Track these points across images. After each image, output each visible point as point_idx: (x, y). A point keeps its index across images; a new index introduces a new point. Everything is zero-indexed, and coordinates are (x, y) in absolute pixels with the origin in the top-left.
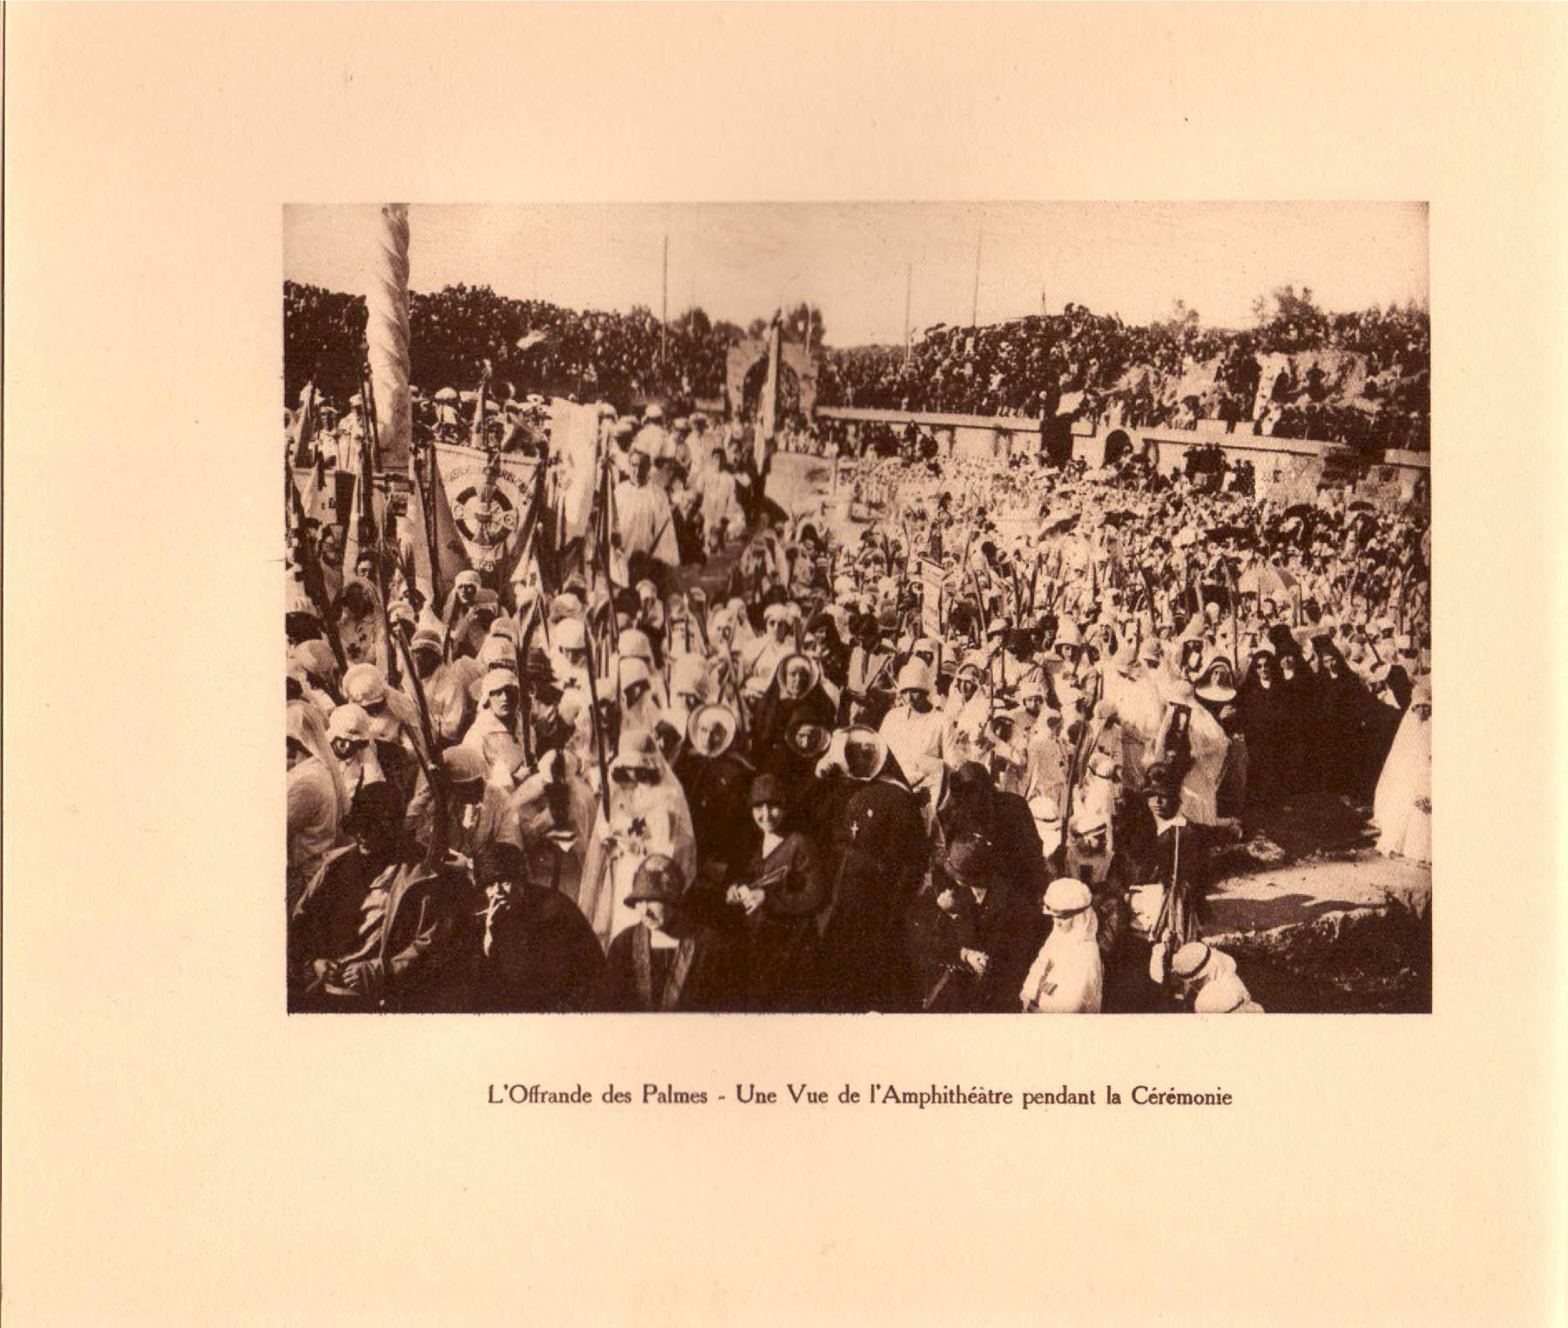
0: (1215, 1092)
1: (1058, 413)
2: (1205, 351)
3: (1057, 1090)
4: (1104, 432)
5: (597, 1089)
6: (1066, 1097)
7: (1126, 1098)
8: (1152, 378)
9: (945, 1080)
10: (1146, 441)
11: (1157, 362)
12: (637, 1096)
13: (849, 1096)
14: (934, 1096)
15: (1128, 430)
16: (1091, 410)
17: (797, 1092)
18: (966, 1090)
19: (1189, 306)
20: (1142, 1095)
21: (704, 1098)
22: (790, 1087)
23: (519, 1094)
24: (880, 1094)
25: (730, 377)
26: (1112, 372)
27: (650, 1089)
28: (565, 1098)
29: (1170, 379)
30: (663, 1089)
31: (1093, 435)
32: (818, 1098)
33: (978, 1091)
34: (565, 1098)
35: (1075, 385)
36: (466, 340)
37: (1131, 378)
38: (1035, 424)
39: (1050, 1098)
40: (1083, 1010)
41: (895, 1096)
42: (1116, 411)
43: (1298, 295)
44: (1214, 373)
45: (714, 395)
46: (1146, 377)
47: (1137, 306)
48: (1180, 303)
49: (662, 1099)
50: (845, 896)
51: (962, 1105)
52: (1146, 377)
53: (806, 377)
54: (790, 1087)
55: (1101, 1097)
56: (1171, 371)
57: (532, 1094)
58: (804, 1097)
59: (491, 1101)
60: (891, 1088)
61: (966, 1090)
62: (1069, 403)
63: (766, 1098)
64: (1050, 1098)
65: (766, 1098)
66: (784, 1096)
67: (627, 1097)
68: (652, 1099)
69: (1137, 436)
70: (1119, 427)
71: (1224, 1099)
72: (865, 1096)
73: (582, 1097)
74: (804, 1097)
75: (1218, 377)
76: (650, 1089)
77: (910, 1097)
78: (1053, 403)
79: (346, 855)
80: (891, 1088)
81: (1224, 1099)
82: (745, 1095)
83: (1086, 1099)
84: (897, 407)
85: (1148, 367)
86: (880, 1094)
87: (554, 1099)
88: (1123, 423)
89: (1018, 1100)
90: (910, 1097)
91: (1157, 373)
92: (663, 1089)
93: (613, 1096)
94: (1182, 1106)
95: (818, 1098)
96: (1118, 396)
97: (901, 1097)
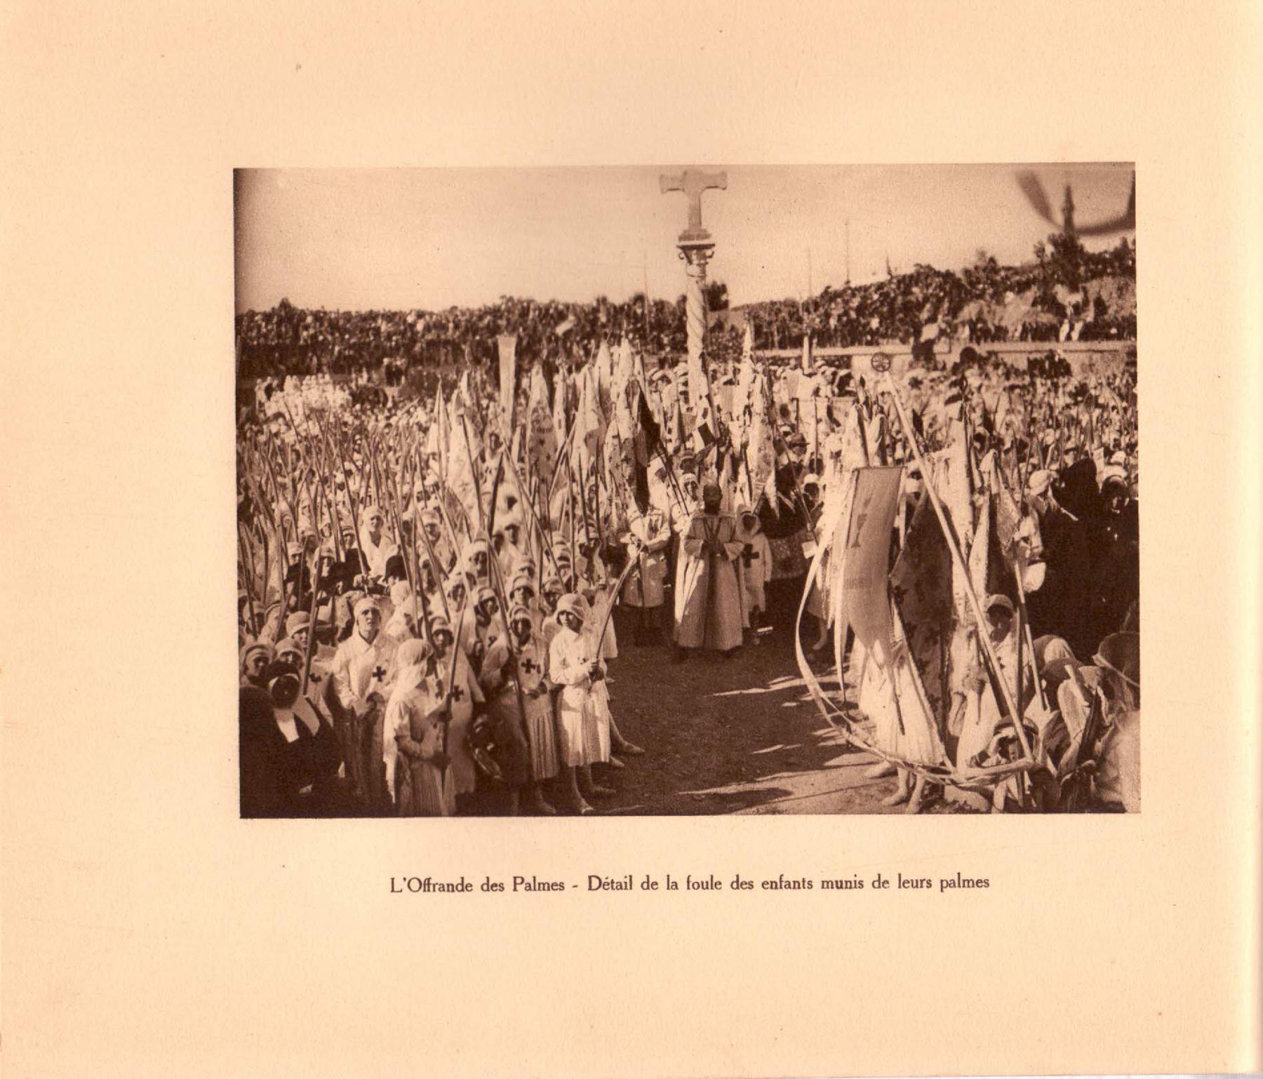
0: (852, 879)
1: (923, 339)
2: (1021, 288)
5: (890, 876)
6: (840, 885)
7: (682, 885)
8: (986, 309)
11: (988, 297)
12: (509, 885)
16: (948, 333)
19: (989, 255)
20: (595, 883)
23: (415, 885)
26: (954, 311)
27: (519, 881)
30: (529, 880)
31: (950, 352)
35: (932, 319)
36: (393, 356)
38: (907, 348)
44: (1031, 300)
49: (528, 888)
50: (711, 711)
51: (546, 893)
55: (663, 884)
57: (426, 885)
59: (590, 889)
62: (929, 332)
67: (501, 887)
68: (521, 888)
70: (968, 345)
71: (982, 883)
73: (465, 887)
75: (1034, 304)
76: (519, 881)
78: (918, 333)
79: (761, 694)
81: (982, 883)
85: (982, 302)
87: (442, 888)
89: (936, 885)
91: (989, 306)
92: (529, 880)
93: (489, 886)
96: (963, 324)
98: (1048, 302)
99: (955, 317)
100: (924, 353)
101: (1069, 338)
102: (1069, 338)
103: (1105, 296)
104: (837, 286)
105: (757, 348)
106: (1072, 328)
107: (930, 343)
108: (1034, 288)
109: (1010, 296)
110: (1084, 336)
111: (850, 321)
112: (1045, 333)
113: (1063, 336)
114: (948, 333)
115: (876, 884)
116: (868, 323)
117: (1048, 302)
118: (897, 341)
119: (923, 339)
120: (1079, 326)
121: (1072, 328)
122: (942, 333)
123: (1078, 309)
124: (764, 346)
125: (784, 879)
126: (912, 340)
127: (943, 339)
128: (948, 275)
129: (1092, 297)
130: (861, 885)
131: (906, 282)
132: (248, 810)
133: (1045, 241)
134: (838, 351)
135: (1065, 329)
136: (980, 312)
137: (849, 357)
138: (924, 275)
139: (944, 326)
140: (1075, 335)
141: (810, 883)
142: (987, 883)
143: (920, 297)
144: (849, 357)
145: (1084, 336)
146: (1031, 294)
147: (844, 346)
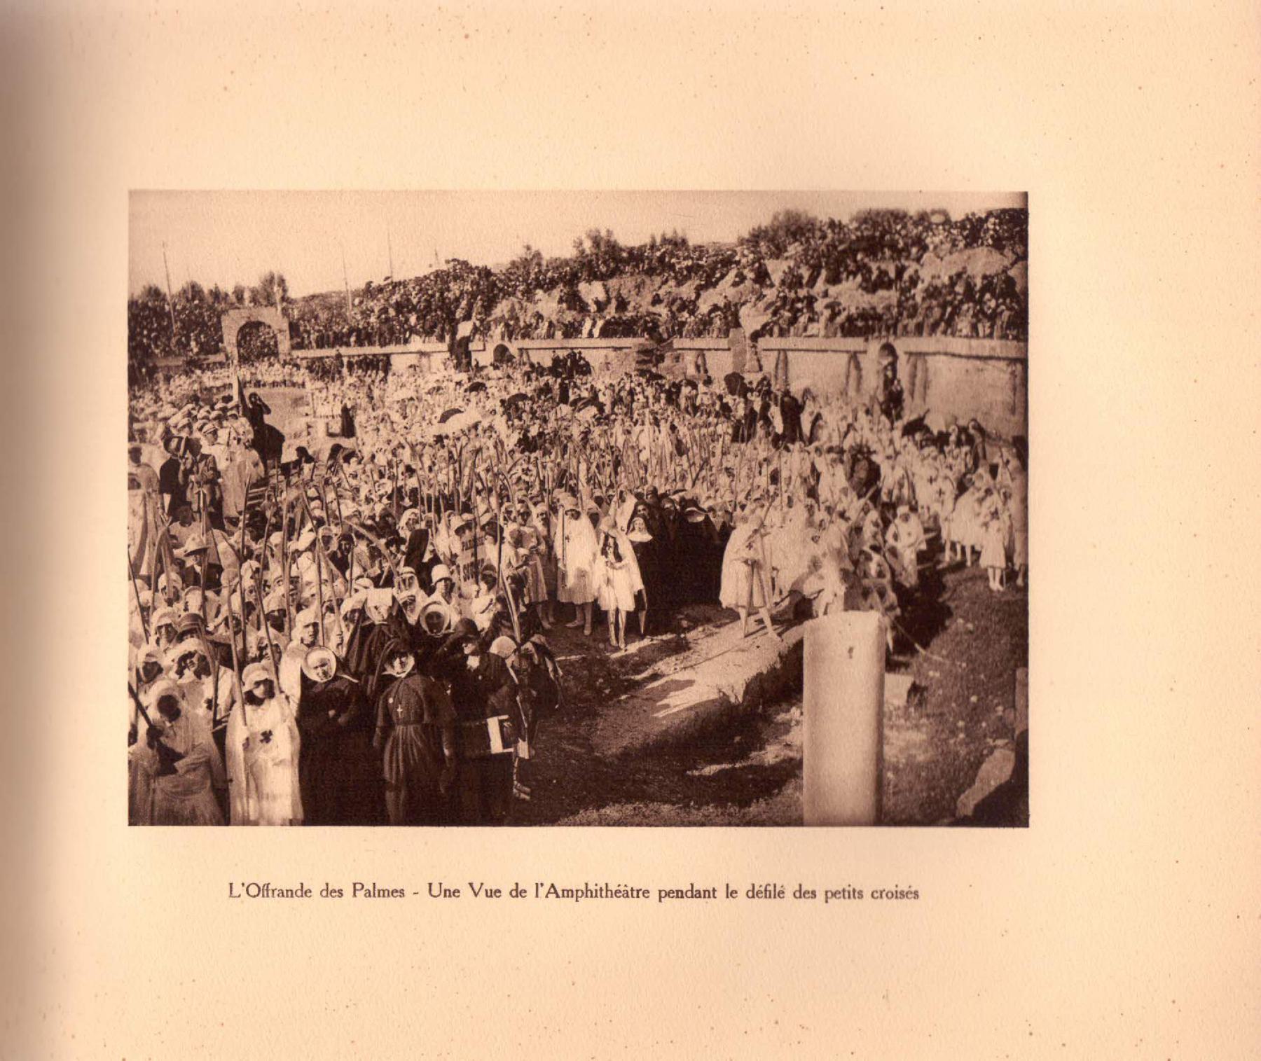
1: (458, 337)
2: (549, 286)
3: (685, 887)
4: (491, 348)
5: (316, 888)
6: (376, 892)
8: (517, 306)
9: (596, 879)
10: (521, 350)
11: (519, 294)
12: (348, 891)
13: (518, 892)
14: (587, 892)
15: (506, 343)
17: (477, 888)
18: (613, 887)
19: (534, 249)
21: (402, 893)
22: (471, 884)
24: (543, 891)
25: (226, 338)
26: (488, 307)
27: (358, 887)
28: (290, 893)
29: (530, 306)
30: (369, 886)
32: (495, 893)
33: (622, 888)
34: (290, 893)
35: (467, 317)
37: (502, 309)
38: (444, 346)
39: (679, 894)
40: (292, 823)
41: (556, 892)
42: (497, 331)
43: (603, 234)
45: (217, 351)
46: (513, 306)
47: (495, 253)
48: (528, 248)
49: (368, 894)
51: (772, 900)
52: (513, 306)
53: (280, 331)
54: (471, 884)
55: (721, 893)
56: (528, 300)
57: (264, 890)
58: (482, 893)
60: (553, 886)
61: (613, 887)
62: (464, 329)
63: (452, 893)
64: (679, 894)
65: (452, 893)
66: (466, 892)
68: (360, 894)
69: (513, 347)
70: (500, 342)
72: (531, 891)
73: (305, 893)
74: (482, 893)
75: (561, 301)
77: (568, 893)
78: (454, 332)
80: (553, 886)
82: (435, 891)
83: (710, 894)
84: (348, 344)
86: (543, 891)
87: (282, 894)
88: (503, 338)
89: (654, 895)
90: (568, 893)
92: (369, 886)
94: (768, 900)
95: (495, 893)
97: (560, 893)
98: (574, 301)
99: (489, 315)
100: (461, 352)
101: (591, 335)
102: (591, 335)
103: (624, 292)
104: (378, 281)
105: (293, 347)
106: (594, 325)
107: (467, 340)
108: (561, 286)
109: (540, 293)
110: (605, 333)
111: (387, 320)
112: (572, 330)
113: (585, 330)
114: (482, 330)
115: (324, 893)
116: (407, 320)
117: (574, 301)
118: (434, 338)
119: (458, 337)
120: (600, 323)
121: (594, 325)
122: (475, 330)
123: (601, 307)
124: (300, 346)
125: (378, 887)
126: (447, 338)
127: (477, 336)
128: (486, 273)
129: (613, 294)
130: (780, 894)
131: (442, 278)
132: (1025, 824)
133: (584, 237)
134: (377, 350)
135: (588, 324)
136: (512, 309)
137: (388, 356)
138: (462, 269)
139: (478, 323)
140: (596, 332)
141: (860, 893)
142: (402, 893)
143: (458, 293)
144: (388, 356)
145: (605, 333)
146: (556, 293)
147: (382, 345)
